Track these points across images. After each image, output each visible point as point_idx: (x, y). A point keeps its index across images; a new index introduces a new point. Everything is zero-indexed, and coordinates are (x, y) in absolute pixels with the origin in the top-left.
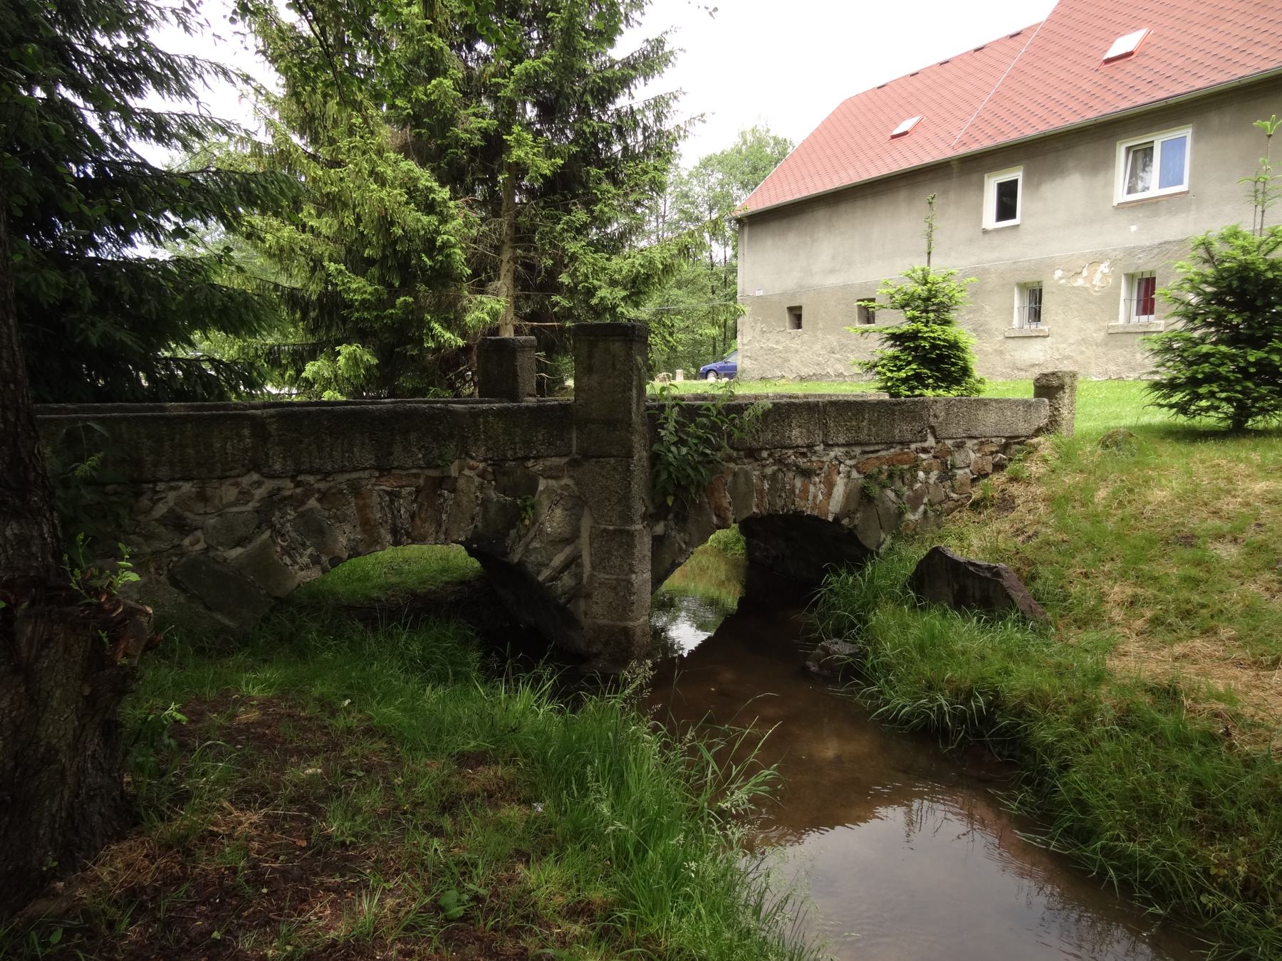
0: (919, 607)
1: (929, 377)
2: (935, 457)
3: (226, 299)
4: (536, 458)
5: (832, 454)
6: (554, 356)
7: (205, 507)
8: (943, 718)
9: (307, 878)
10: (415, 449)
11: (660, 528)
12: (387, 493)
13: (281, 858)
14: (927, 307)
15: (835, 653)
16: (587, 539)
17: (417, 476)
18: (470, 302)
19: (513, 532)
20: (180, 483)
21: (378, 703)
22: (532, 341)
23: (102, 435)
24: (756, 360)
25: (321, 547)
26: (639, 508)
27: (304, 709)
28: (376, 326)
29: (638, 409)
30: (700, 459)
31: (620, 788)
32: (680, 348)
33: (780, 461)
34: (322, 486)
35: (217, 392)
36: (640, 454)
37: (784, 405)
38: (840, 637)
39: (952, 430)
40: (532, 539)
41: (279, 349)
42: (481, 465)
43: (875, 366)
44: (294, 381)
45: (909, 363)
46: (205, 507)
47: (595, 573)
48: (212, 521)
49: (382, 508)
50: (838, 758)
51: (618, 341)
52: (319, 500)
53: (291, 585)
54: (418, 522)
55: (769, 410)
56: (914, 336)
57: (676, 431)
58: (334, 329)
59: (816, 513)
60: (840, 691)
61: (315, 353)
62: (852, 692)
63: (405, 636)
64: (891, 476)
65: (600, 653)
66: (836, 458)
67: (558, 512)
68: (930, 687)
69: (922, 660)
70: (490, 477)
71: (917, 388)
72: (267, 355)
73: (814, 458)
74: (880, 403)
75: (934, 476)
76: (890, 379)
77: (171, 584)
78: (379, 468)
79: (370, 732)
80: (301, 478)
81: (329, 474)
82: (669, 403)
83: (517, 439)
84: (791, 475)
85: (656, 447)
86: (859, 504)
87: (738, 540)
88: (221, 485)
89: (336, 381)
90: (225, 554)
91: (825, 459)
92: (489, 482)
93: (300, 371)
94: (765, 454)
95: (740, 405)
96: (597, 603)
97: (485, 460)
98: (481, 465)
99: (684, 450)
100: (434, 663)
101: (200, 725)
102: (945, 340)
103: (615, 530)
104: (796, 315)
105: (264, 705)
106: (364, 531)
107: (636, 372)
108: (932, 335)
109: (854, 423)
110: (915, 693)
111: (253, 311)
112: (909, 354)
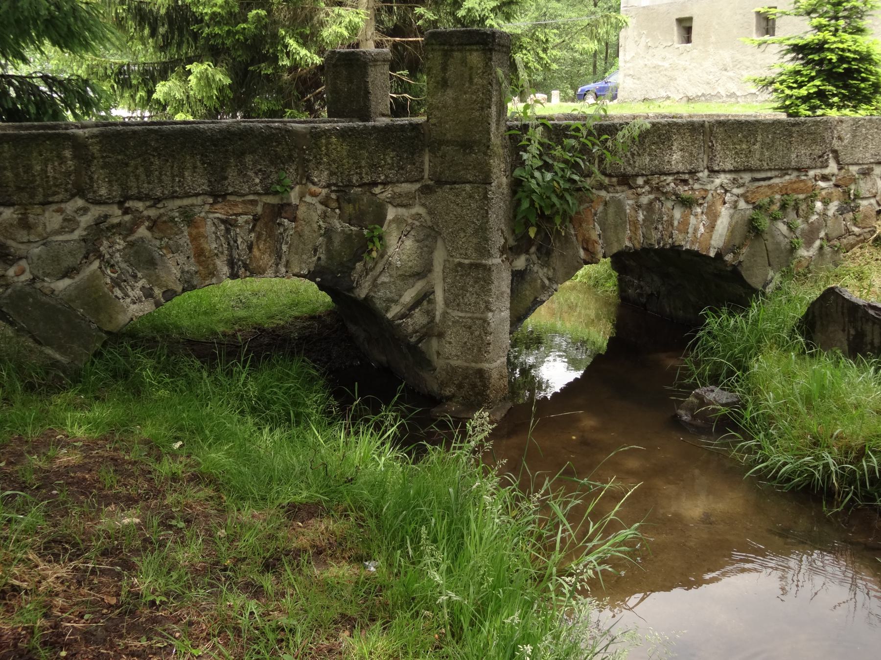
0: (809, 352)
1: (834, 95)
2: (836, 186)
4: (384, 184)
5: (718, 182)
6: (419, 75)
7: (28, 235)
8: (829, 477)
9: (110, 640)
10: (251, 174)
11: (520, 263)
12: (223, 221)
13: (86, 617)
14: (837, 12)
15: (711, 403)
16: (441, 274)
17: (254, 203)
18: (327, 15)
19: (359, 266)
21: (210, 446)
22: (386, 54)
24: (639, 79)
25: (155, 281)
26: (498, 240)
27: (128, 451)
28: (228, 42)
29: (497, 129)
30: (567, 186)
31: (457, 551)
32: (555, 66)
33: (657, 189)
34: (152, 213)
35: (50, 112)
36: (500, 180)
37: (664, 125)
38: (717, 385)
39: (858, 155)
40: (381, 273)
42: (324, 191)
43: (772, 83)
44: (148, 101)
45: (812, 79)
46: (28, 235)
47: (449, 311)
48: (37, 251)
49: (217, 238)
50: (707, 519)
51: (477, 50)
52: (150, 229)
53: (122, 319)
54: (256, 252)
55: (648, 131)
56: (820, 47)
57: (541, 155)
58: (185, 46)
59: (696, 247)
60: (716, 443)
61: (166, 73)
62: (727, 445)
63: (244, 375)
64: (784, 207)
65: (454, 396)
66: (722, 186)
67: (409, 243)
68: (816, 443)
69: (808, 413)
70: (334, 205)
71: (819, 107)
73: (696, 186)
74: (776, 123)
75: (833, 207)
76: (789, 97)
78: (212, 194)
80: (129, 204)
81: (158, 200)
83: (363, 163)
84: (669, 204)
85: (518, 172)
86: (746, 238)
87: (610, 276)
88: (44, 211)
89: (189, 103)
90: (53, 286)
91: (708, 187)
92: (333, 210)
93: (150, 92)
94: (640, 181)
95: (614, 125)
96: (450, 343)
97: (328, 186)
98: (324, 191)
99: (549, 176)
100: (274, 403)
101: (17, 468)
102: (855, 52)
103: (471, 265)
104: (686, 27)
105: (89, 446)
106: (199, 263)
107: (495, 87)
108: (841, 46)
109: (744, 146)
110: (798, 449)
111: (82, 21)
112: (812, 69)
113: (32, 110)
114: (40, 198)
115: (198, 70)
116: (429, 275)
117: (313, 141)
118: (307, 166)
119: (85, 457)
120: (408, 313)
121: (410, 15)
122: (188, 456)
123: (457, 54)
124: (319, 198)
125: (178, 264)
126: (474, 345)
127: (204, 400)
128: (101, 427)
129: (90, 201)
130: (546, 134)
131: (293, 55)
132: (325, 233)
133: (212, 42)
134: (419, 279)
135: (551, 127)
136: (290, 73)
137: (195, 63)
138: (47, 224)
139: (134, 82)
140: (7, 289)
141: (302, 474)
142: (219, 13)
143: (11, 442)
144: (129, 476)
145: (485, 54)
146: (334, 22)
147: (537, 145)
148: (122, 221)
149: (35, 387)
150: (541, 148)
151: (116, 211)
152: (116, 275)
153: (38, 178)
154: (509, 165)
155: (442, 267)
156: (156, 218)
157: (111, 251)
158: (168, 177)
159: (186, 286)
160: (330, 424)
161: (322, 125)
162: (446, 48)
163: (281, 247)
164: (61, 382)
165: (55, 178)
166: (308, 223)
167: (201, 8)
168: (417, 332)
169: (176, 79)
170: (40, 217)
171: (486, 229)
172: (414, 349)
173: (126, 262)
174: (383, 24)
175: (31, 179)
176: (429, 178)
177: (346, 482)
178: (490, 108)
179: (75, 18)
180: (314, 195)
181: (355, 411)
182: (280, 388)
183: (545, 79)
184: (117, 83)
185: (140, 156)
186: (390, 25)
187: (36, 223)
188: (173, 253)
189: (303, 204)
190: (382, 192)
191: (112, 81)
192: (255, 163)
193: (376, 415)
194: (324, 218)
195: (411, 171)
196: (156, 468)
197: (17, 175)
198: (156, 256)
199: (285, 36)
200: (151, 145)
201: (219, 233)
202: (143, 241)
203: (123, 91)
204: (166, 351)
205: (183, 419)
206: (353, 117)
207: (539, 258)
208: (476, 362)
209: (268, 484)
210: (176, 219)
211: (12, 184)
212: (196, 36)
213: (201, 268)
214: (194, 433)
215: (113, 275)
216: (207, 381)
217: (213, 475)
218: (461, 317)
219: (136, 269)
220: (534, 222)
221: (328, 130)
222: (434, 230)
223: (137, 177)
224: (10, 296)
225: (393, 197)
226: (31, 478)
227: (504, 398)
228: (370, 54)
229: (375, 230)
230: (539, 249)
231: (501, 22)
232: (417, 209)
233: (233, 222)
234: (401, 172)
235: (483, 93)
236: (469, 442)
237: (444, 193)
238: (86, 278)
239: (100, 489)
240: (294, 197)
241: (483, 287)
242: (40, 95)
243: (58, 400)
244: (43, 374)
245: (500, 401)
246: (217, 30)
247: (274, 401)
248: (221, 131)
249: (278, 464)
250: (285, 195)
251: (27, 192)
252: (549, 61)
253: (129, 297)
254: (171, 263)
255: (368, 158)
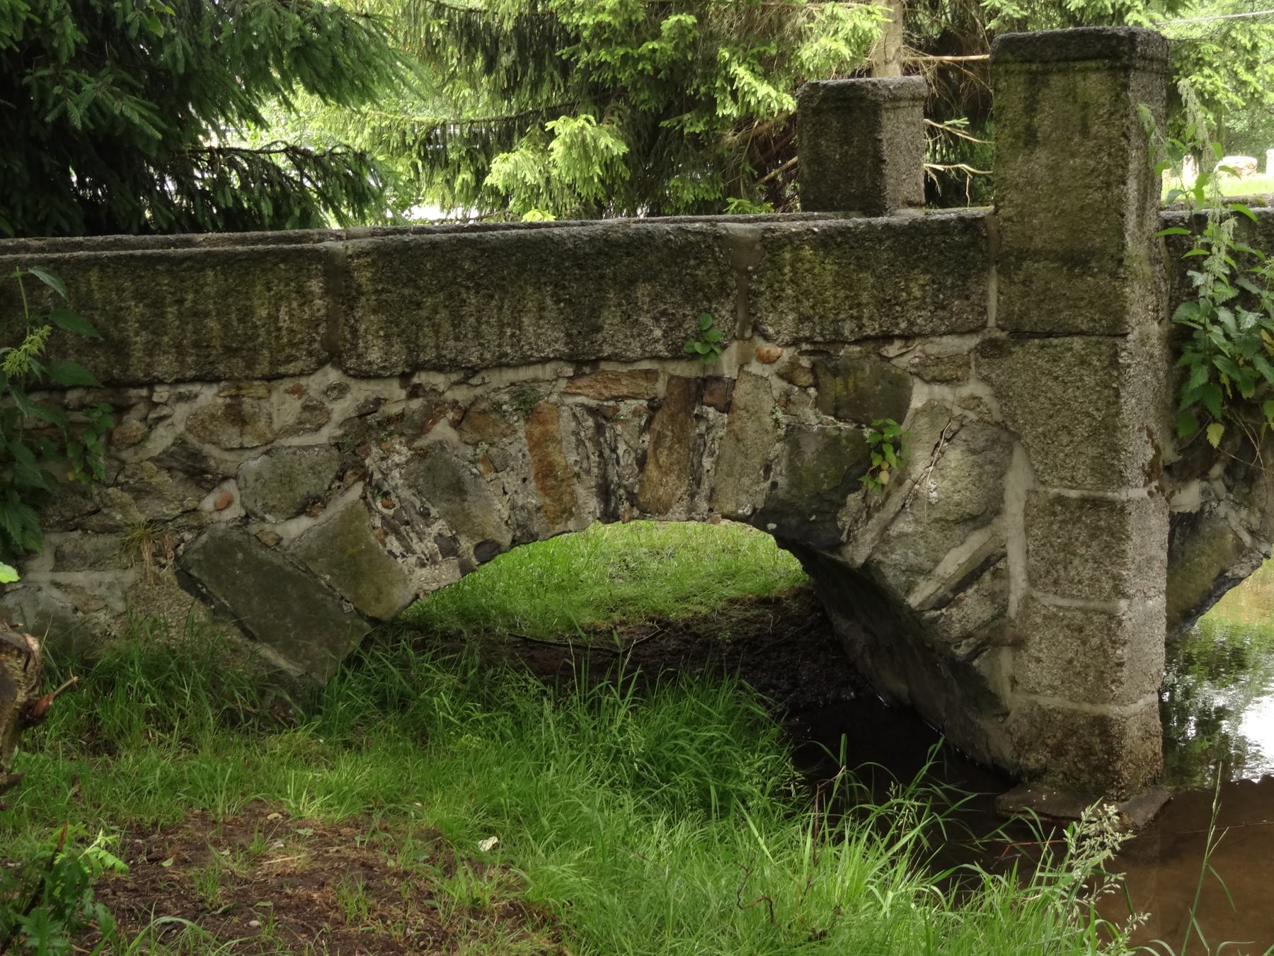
3: (308, 28)
4: (907, 337)
10: (646, 319)
11: (1189, 498)
12: (591, 411)
16: (1020, 519)
17: (650, 375)
18: (811, 18)
19: (853, 500)
20: (196, 388)
21: (547, 850)
23: (55, 294)
25: (460, 522)
26: (1140, 451)
28: (624, 77)
29: (1141, 224)
35: (297, 212)
40: (897, 514)
41: (443, 132)
42: (787, 354)
44: (476, 190)
47: (1037, 594)
49: (580, 443)
51: (1098, 69)
52: (456, 425)
53: (400, 596)
54: (651, 469)
57: (1232, 278)
58: (546, 87)
61: (510, 137)
63: (623, 711)
65: (1045, 770)
67: (955, 456)
70: (806, 379)
72: (423, 144)
77: (183, 586)
78: (570, 359)
79: (518, 913)
80: (419, 378)
81: (473, 371)
82: (1214, 211)
83: (865, 297)
85: (1184, 312)
88: (270, 391)
89: (550, 192)
90: (279, 530)
92: (804, 389)
93: (481, 174)
96: (1039, 660)
97: (795, 343)
99: (1250, 319)
100: (680, 769)
103: (1084, 500)
105: (322, 839)
106: (544, 490)
113: (267, 208)
114: (263, 368)
115: (568, 130)
116: (995, 520)
117: (767, 256)
118: (755, 303)
119: (316, 859)
120: (951, 596)
121: (974, 13)
122: (505, 868)
123: (1057, 81)
124: (775, 367)
125: (505, 493)
126: (1087, 666)
127: (543, 757)
128: (348, 802)
129: (352, 372)
130: (1244, 234)
131: (744, 97)
132: (786, 436)
133: (594, 78)
134: (975, 529)
135: (1254, 219)
136: (738, 130)
137: (562, 118)
138: (274, 416)
139: (453, 156)
140: (199, 535)
141: (723, 916)
142: (609, 25)
143: (188, 821)
144: (391, 900)
145: (1114, 76)
146: (824, 31)
147: (1223, 256)
148: (407, 411)
149: (239, 719)
150: (1233, 263)
151: (395, 391)
152: (391, 512)
153: (262, 331)
154: (1166, 298)
155: (1022, 505)
156: (467, 404)
157: (384, 465)
158: (492, 327)
159: (518, 534)
160: (788, 817)
161: (784, 225)
162: (1034, 67)
163: (700, 462)
164: (286, 713)
165: (291, 331)
166: (755, 415)
167: (577, 15)
168: (968, 635)
169: (527, 148)
170: (263, 403)
171: (1115, 428)
172: (962, 670)
173: (410, 487)
174: (919, 32)
175: (250, 333)
176: (998, 326)
177: (810, 939)
178: (1124, 183)
179: (346, 41)
180: (767, 360)
181: (841, 792)
182: (692, 740)
183: (1252, 127)
184: (424, 158)
185: (442, 289)
186: (935, 32)
187: (255, 413)
188: (497, 471)
189: (745, 378)
190: (902, 355)
191: (414, 155)
192: (656, 298)
193: (880, 805)
194: (786, 406)
195: (962, 311)
196: (444, 887)
197: (226, 326)
198: (466, 476)
199: (730, 61)
200: (463, 269)
201: (582, 434)
202: (443, 449)
203: (432, 173)
204: (477, 659)
205: (501, 793)
206: (851, 209)
207: (1229, 489)
208: (1092, 702)
209: (656, 933)
210: (505, 407)
211: (217, 343)
212: (565, 68)
213: (548, 501)
214: (519, 821)
215: (385, 511)
216: (550, 721)
217: (550, 909)
218: (1060, 608)
219: (428, 500)
220: (1217, 413)
221: (798, 234)
222: (1006, 429)
223: (436, 329)
224: (204, 546)
225: (923, 365)
226: (216, 895)
227: (1154, 781)
228: (886, 87)
229: (885, 430)
230: (1229, 471)
231: (1157, 16)
232: (974, 387)
233: (610, 414)
234: (941, 313)
235: (1109, 154)
236: (1070, 869)
237: (1027, 354)
238: (338, 516)
239: (338, 924)
240: (727, 364)
241: (1108, 545)
242: (280, 184)
243: (276, 744)
244: (254, 694)
245: (1145, 785)
246: (604, 55)
247: (680, 765)
248: (592, 239)
249: (678, 894)
250: (708, 361)
251: (242, 357)
252: (1260, 88)
253: (414, 553)
254: (491, 491)
255: (873, 287)
